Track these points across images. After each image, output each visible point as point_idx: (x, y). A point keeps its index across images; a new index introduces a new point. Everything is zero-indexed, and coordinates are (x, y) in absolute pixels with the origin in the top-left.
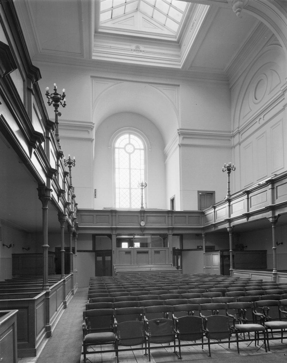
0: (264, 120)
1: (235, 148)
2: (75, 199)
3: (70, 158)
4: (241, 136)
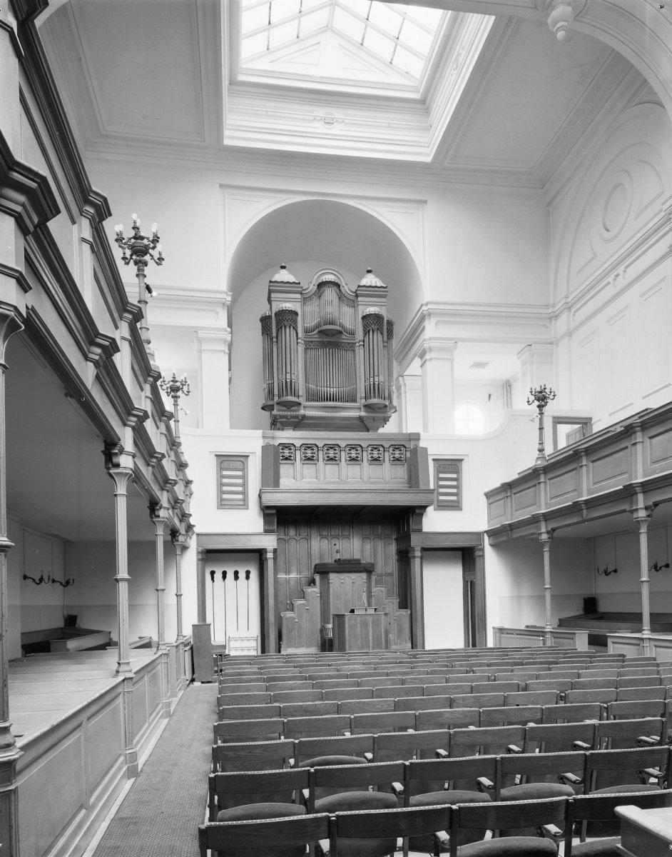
0: (615, 286)
1: (571, 336)
2: (187, 471)
3: (174, 378)
4: (574, 315)
